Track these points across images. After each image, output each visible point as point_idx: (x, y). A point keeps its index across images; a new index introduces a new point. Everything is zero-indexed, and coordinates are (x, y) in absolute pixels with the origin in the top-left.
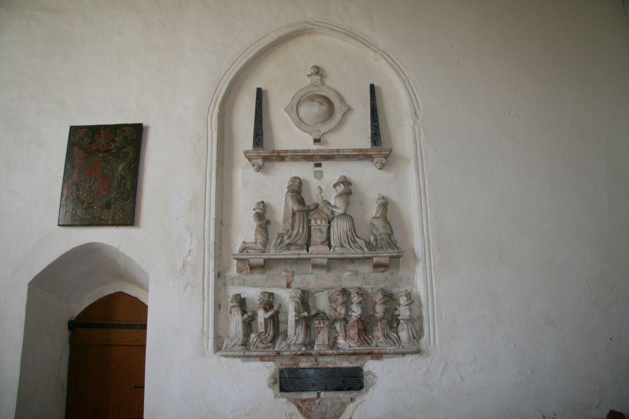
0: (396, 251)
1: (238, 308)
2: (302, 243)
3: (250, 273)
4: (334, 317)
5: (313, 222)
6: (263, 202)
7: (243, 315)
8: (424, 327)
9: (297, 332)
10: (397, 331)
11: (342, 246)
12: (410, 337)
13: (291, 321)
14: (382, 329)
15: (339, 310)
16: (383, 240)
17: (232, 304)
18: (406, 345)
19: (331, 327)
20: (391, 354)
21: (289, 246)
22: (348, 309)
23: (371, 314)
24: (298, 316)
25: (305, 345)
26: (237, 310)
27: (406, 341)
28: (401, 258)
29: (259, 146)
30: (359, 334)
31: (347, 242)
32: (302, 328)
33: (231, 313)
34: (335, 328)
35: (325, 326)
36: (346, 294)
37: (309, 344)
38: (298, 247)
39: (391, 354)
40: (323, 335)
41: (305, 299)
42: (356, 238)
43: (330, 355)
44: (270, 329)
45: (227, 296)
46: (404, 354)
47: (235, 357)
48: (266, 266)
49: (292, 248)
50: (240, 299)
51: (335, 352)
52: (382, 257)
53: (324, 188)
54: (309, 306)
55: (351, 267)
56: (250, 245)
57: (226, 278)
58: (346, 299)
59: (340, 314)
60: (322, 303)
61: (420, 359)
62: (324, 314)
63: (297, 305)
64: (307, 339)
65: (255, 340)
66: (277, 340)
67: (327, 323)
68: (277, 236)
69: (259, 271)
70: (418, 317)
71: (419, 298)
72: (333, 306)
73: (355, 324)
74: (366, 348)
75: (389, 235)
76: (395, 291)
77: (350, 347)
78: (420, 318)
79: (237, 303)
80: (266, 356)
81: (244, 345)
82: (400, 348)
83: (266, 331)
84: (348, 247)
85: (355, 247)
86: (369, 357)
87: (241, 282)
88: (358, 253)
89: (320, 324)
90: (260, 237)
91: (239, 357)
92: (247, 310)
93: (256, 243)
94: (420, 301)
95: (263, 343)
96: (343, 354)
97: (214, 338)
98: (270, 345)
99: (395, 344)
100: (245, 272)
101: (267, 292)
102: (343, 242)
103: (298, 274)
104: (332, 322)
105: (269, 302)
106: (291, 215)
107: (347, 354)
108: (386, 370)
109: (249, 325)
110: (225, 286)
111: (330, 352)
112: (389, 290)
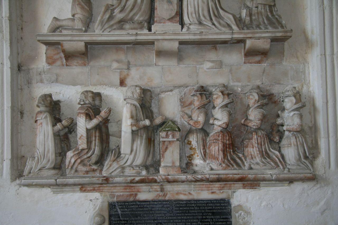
0: (280, 29)
1: (47, 114)
2: (141, 19)
3: (67, 65)
4: (188, 127)
7: (54, 125)
8: (319, 143)
9: (135, 148)
10: (280, 147)
11: (200, 23)
12: (300, 157)
13: (125, 132)
14: (258, 144)
15: (195, 117)
16: (262, 15)
17: (39, 109)
18: (295, 167)
19: (184, 141)
20: (272, 180)
21: (121, 23)
22: (208, 116)
23: (243, 121)
24: (135, 125)
25: (147, 168)
26: (46, 117)
27: (295, 161)
28: (286, 43)
30: (224, 151)
31: (208, 18)
32: (141, 143)
33: (36, 121)
34: (189, 143)
35: (175, 139)
36: (205, 94)
37: (152, 166)
38: (136, 26)
39: (272, 180)
40: (173, 152)
41: (146, 102)
42: (221, 11)
43: (183, 182)
44: (95, 144)
45: (33, 99)
46: (291, 181)
47: (42, 186)
48: (89, 52)
49: (127, 26)
50: (51, 103)
51: (190, 177)
52: (260, 39)
54: (152, 112)
55: (212, 55)
56: (64, 23)
57: (31, 71)
58: (205, 101)
59: (197, 122)
60: (171, 107)
61: (315, 188)
62: (174, 122)
63: (134, 109)
64: (150, 158)
65: (73, 161)
66: (106, 160)
67: (178, 135)
68: (103, 9)
69: (80, 62)
70: (310, 128)
71: (312, 101)
72: (187, 111)
73: (219, 136)
74: (235, 172)
75: (270, 6)
76: (276, 90)
77: (212, 169)
78: (314, 128)
79: (46, 106)
80: (88, 184)
81: (57, 169)
82: (285, 172)
83: (89, 148)
84: (209, 24)
85: (220, 23)
86: (240, 184)
87: (54, 78)
88: (224, 33)
89: (167, 136)
90: (78, 10)
91: (49, 186)
92: (63, 118)
93: (73, 20)
94: (314, 105)
95: (84, 165)
96: (201, 180)
97: (12, 160)
98: (95, 167)
99: (278, 166)
100: (59, 63)
101: (90, 91)
102: (202, 17)
103: (136, 65)
104: (184, 134)
105: (94, 106)
107: (208, 180)
108: (264, 204)
109: (64, 139)
110: (29, 83)
111: (183, 177)
112: (268, 88)
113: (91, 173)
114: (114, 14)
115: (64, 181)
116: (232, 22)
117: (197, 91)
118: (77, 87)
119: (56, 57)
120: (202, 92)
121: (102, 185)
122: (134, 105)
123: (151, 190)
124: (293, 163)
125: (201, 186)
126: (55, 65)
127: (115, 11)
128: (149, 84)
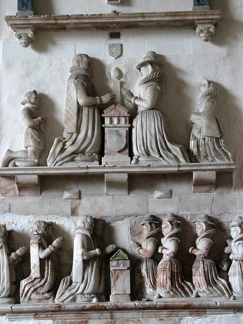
3: (19, 196)
5: (107, 121)
6: (35, 92)
7: (9, 255)
11: (148, 154)
22: (158, 244)
29: (27, 8)
31: (156, 150)
35: (126, 268)
49: (78, 158)
53: (124, 71)
60: (123, 236)
63: (85, 239)
65: (26, 289)
75: (217, 139)
82: (231, 299)
83: (42, 276)
84: (157, 156)
86: (186, 312)
87: (7, 208)
89: (118, 265)
93: (26, 152)
98: (47, 295)
100: (12, 193)
106: (76, 111)
113: (44, 301)
114: (65, 147)
115: (20, 308)
116: (177, 152)
117: (147, 221)
118: (29, 216)
119: (9, 187)
120: (152, 222)
121: (55, 313)
122: (87, 236)
123: (101, 317)
124: (238, 291)
125: (150, 313)
126: (7, 195)
127: (67, 144)
128: (100, 213)
